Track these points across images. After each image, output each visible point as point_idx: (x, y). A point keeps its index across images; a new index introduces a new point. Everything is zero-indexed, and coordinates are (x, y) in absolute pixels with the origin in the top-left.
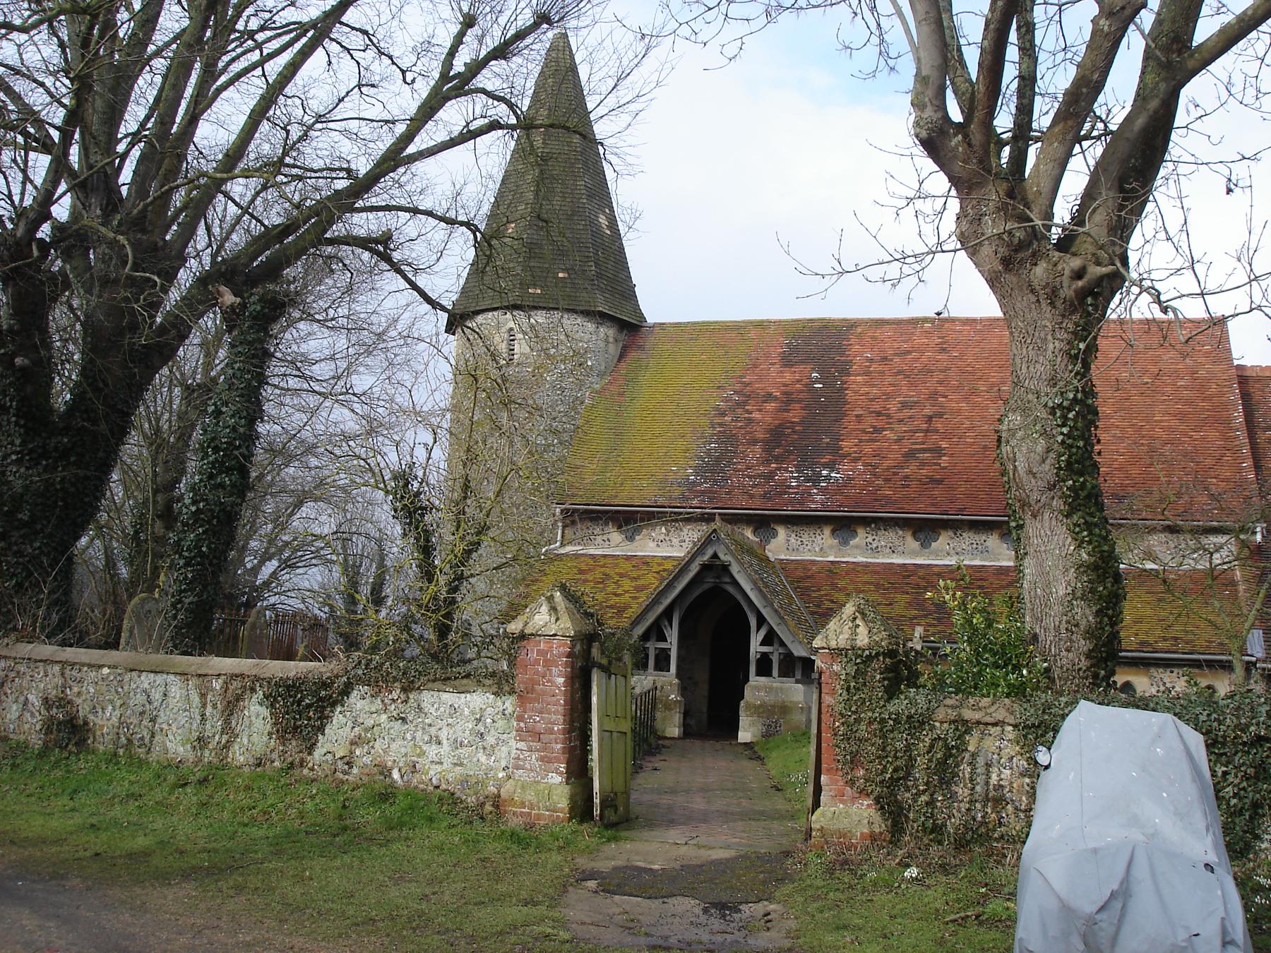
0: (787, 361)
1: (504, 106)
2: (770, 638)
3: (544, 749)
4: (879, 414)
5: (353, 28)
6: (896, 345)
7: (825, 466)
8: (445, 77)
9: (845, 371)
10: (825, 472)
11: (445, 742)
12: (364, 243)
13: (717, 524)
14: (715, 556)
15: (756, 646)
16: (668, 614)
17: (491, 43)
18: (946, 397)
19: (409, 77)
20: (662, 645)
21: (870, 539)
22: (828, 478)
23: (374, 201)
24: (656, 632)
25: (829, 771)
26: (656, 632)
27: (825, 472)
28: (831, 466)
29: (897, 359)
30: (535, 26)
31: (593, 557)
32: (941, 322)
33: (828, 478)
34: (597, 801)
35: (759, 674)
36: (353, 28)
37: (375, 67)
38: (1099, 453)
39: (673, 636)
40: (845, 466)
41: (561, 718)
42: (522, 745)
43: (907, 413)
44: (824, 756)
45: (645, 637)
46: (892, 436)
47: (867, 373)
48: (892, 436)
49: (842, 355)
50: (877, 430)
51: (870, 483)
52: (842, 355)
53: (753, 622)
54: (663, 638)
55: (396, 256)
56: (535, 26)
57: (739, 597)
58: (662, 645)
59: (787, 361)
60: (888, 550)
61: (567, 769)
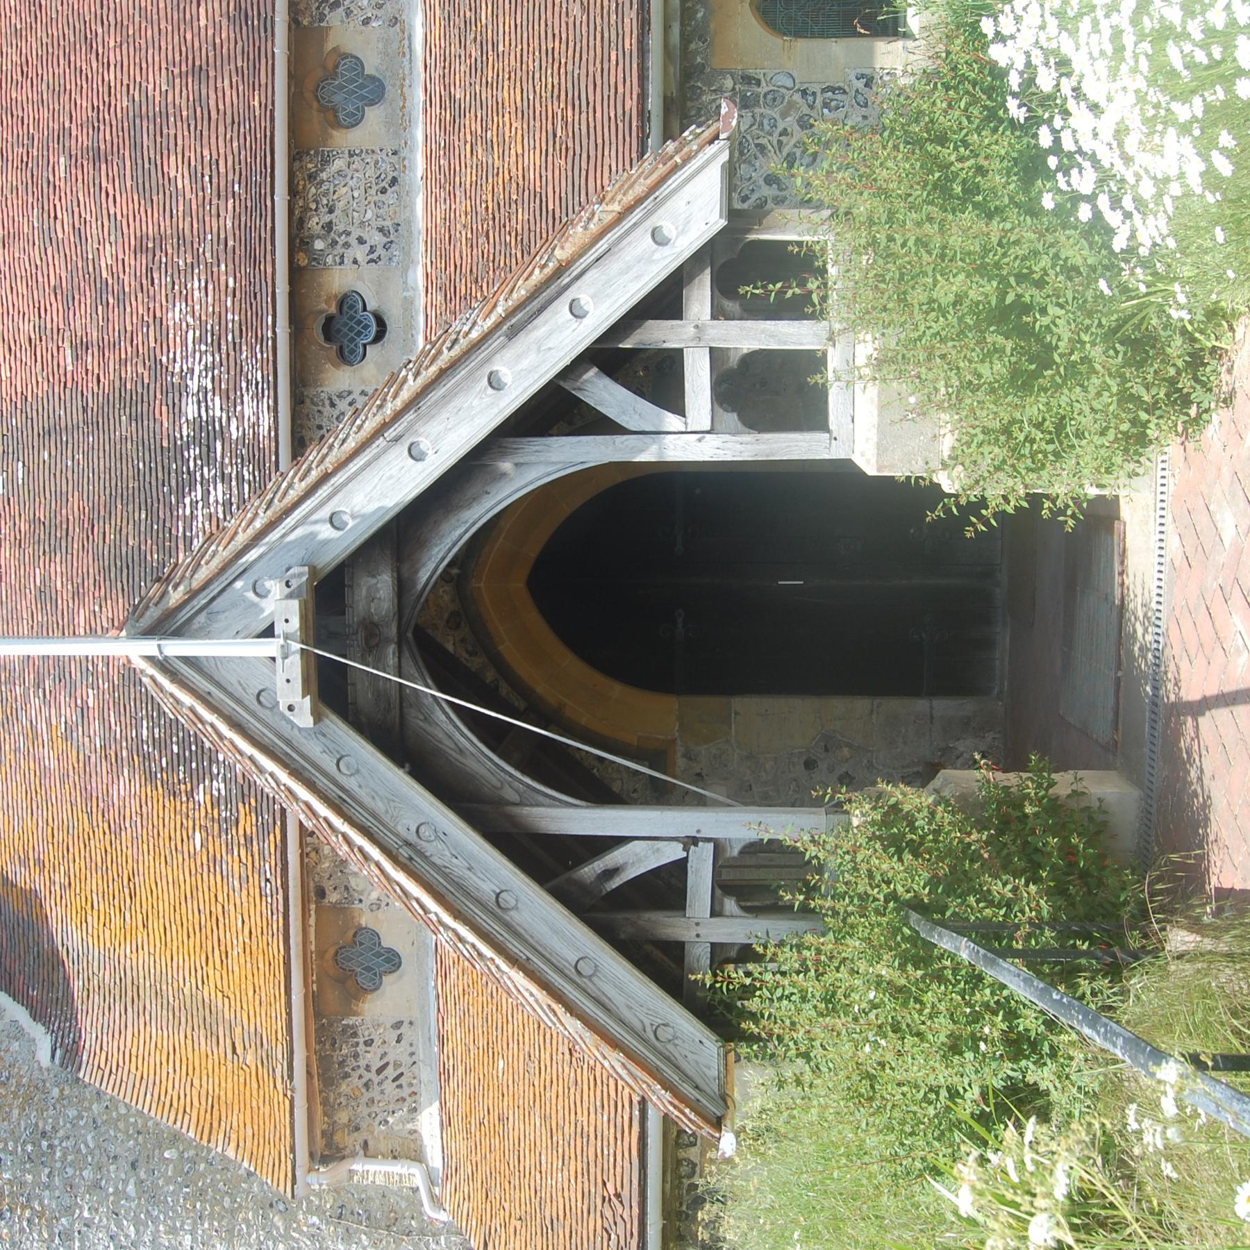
21: (360, 253)
27: (191, 410)
33: (202, 398)
60: (390, 197)
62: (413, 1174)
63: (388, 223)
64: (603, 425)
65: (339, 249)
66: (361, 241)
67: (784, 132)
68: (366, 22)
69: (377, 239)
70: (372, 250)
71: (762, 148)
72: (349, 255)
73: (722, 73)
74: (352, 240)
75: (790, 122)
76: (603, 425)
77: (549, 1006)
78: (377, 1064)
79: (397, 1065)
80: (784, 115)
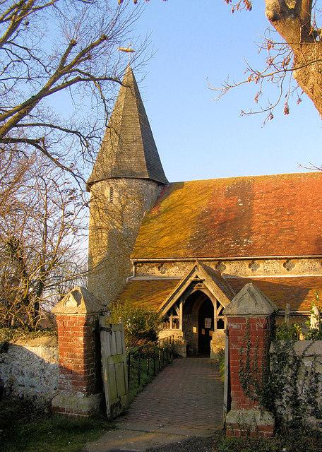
1: (77, 73)
3: (75, 378)
4: (267, 215)
5: (21, 47)
7: (245, 237)
8: (61, 66)
10: (245, 240)
11: (25, 374)
12: (34, 143)
13: (196, 263)
14: (197, 277)
16: (177, 303)
19: (48, 69)
20: (176, 317)
23: (26, 122)
24: (172, 311)
25: (235, 389)
26: (172, 311)
27: (245, 240)
28: (248, 237)
30: (101, 41)
31: (148, 281)
35: (218, 328)
36: (21, 47)
37: (36, 67)
38: (270, 45)
39: (180, 311)
40: (254, 236)
41: (82, 360)
42: (62, 376)
44: (232, 379)
45: (169, 313)
46: (273, 223)
47: (261, 198)
50: (266, 222)
54: (175, 314)
55: (49, 150)
56: (101, 41)
57: (208, 294)
58: (176, 317)
61: (87, 389)
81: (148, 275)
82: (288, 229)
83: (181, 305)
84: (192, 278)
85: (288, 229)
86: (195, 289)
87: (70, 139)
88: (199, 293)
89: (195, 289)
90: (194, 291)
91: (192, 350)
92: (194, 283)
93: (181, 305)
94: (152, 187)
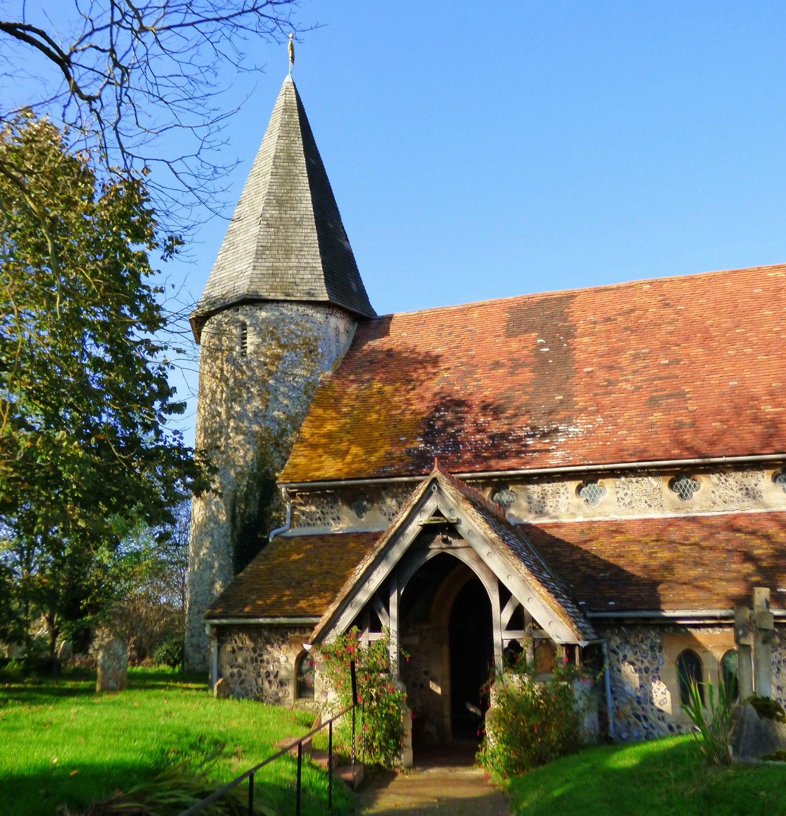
0: (510, 333)
2: (519, 619)
6: (619, 307)
9: (569, 334)
14: (438, 513)
15: (501, 637)
16: (382, 595)
17: (166, 25)
18: (679, 345)
21: (621, 494)
22: (566, 433)
29: (620, 319)
32: (548, 483)
34: (777, 410)
39: (390, 621)
43: (640, 364)
46: (629, 387)
47: (592, 334)
48: (629, 387)
49: (565, 320)
51: (613, 433)
52: (565, 320)
53: (495, 599)
54: (376, 627)
59: (510, 333)
60: (644, 505)
62: (286, 527)
63: (633, 505)
64: (502, 606)
65: (622, 486)
66: (626, 494)
67: (642, 662)
68: (713, 492)
69: (627, 500)
70: (623, 499)
71: (636, 653)
72: (620, 490)
73: (662, 639)
74: (626, 491)
75: (647, 664)
76: (502, 606)
77: (176, 797)
78: (324, 511)
79: (324, 518)
80: (649, 662)
81: (253, 465)
82: (669, 396)
83: (394, 599)
84: (422, 519)
85: (669, 396)
86: (436, 547)
87: (160, 125)
88: (448, 562)
89: (436, 547)
90: (430, 555)
91: (432, 729)
92: (428, 531)
93: (394, 599)
94: (338, 323)
